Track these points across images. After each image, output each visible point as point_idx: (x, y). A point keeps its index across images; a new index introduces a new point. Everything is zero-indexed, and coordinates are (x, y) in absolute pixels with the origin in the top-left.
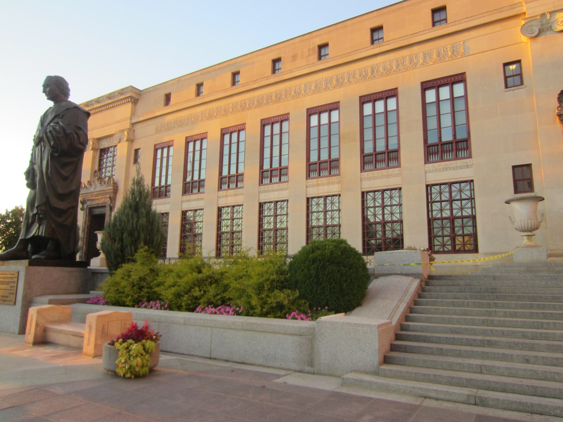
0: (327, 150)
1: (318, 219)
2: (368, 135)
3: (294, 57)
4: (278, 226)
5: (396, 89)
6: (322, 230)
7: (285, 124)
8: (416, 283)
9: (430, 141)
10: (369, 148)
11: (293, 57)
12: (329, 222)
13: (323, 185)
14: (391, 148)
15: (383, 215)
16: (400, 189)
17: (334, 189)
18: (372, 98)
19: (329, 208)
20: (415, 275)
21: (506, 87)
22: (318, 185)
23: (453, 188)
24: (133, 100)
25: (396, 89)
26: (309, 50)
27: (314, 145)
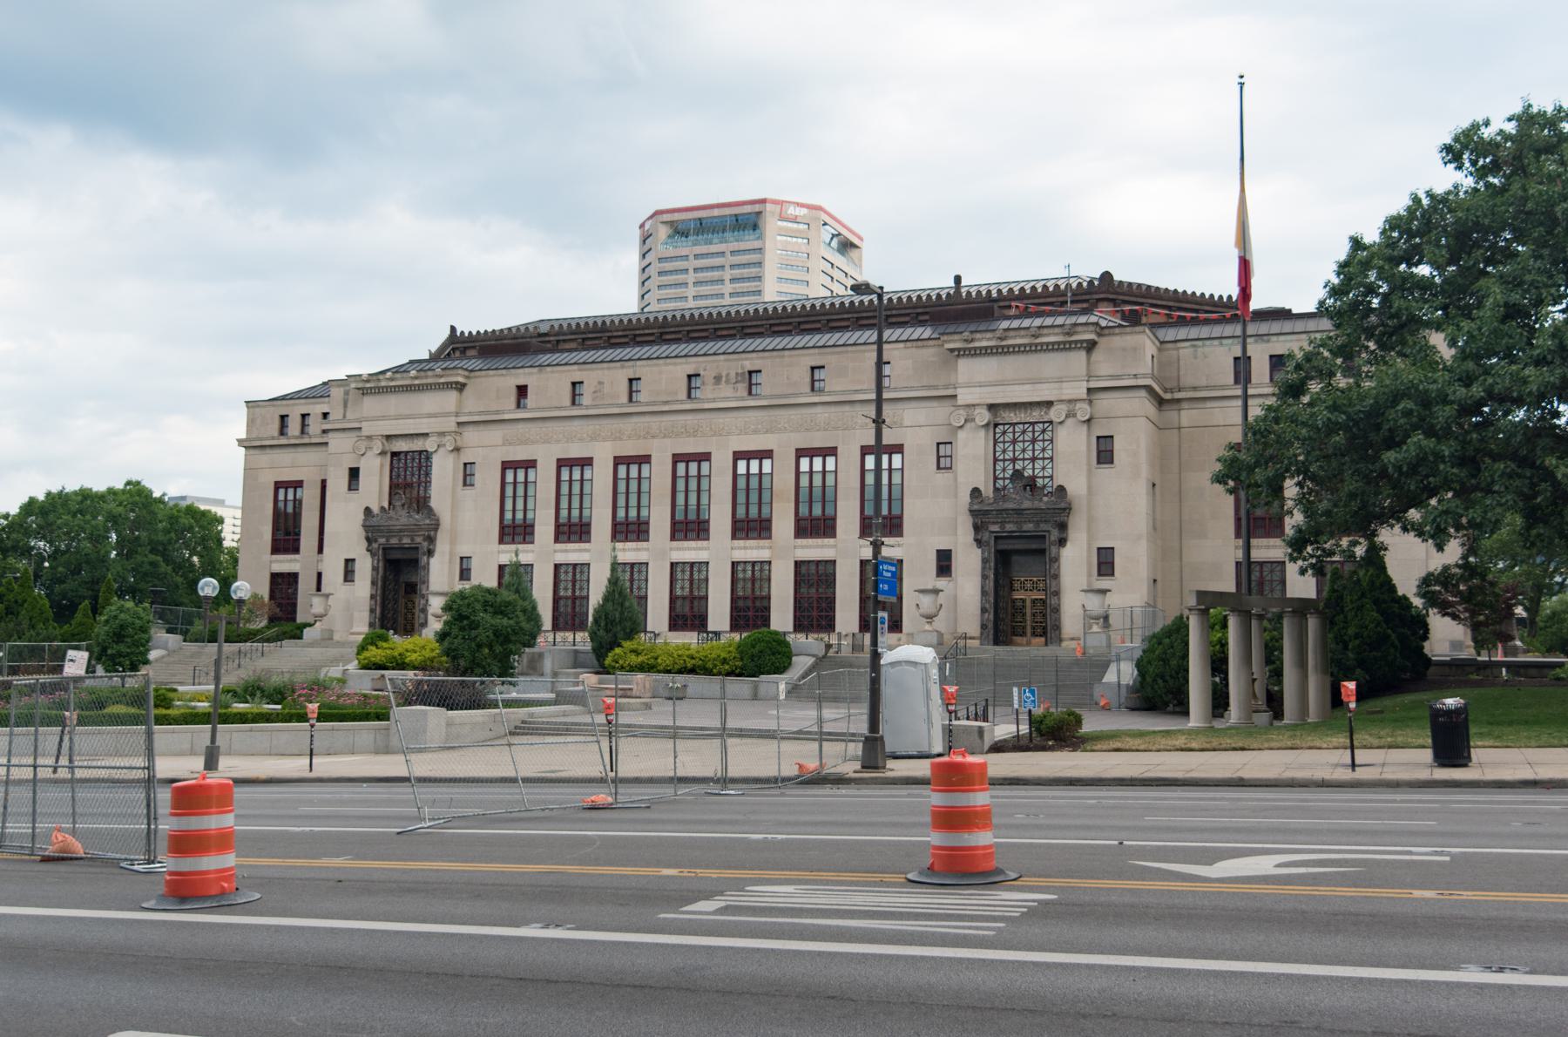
0: (744, 507)
1: (566, 589)
2: (621, 501)
3: (718, 379)
4: (577, 593)
5: (592, 458)
6: (570, 602)
7: (531, 472)
8: (813, 659)
9: (866, 513)
10: (680, 516)
11: (715, 378)
12: (758, 593)
13: (751, 548)
14: (763, 516)
15: (753, 590)
16: (770, 562)
17: (641, 557)
18: (811, 453)
19: (578, 577)
20: (813, 656)
21: (939, 468)
22: (745, 548)
23: (1265, 569)
24: (1085, 345)
25: (592, 458)
26: (737, 374)
27: (621, 501)
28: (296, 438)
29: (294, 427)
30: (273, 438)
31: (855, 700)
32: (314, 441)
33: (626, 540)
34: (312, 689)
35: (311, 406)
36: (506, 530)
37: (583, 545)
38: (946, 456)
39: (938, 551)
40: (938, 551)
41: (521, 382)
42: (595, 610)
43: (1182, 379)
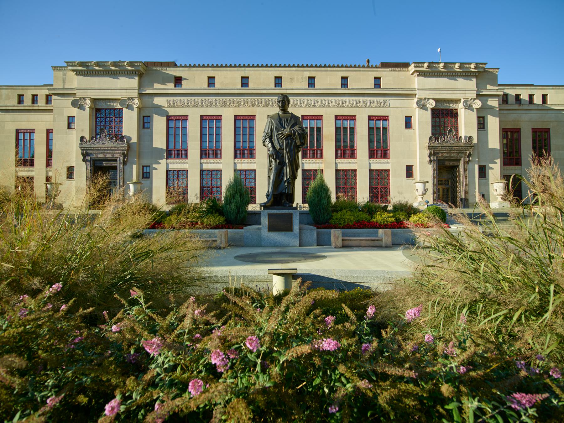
17: (321, 166)
28: (29, 106)
29: (27, 100)
30: (14, 106)
31: (330, 234)
32: (41, 108)
33: (242, 158)
34: (518, 217)
35: (38, 91)
36: (238, 152)
37: (218, 160)
38: (147, 123)
39: (407, 166)
40: (407, 166)
41: (378, 75)
42: (228, 190)
43: (185, 81)
